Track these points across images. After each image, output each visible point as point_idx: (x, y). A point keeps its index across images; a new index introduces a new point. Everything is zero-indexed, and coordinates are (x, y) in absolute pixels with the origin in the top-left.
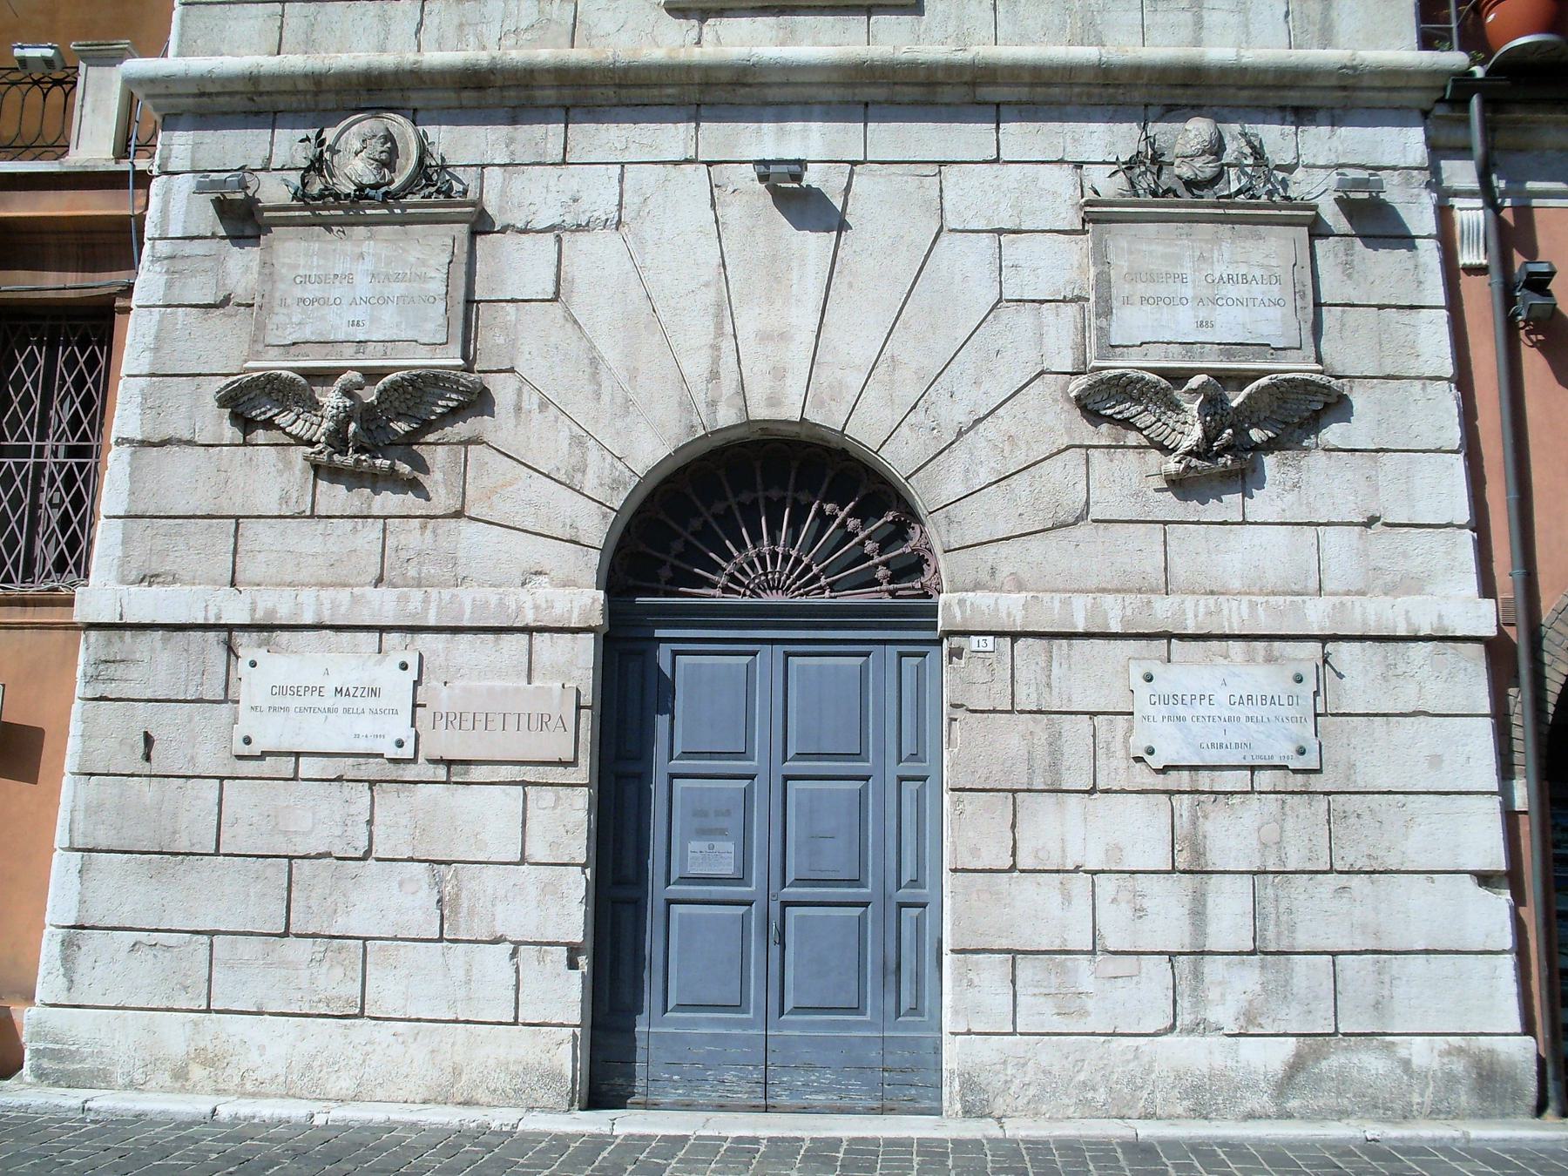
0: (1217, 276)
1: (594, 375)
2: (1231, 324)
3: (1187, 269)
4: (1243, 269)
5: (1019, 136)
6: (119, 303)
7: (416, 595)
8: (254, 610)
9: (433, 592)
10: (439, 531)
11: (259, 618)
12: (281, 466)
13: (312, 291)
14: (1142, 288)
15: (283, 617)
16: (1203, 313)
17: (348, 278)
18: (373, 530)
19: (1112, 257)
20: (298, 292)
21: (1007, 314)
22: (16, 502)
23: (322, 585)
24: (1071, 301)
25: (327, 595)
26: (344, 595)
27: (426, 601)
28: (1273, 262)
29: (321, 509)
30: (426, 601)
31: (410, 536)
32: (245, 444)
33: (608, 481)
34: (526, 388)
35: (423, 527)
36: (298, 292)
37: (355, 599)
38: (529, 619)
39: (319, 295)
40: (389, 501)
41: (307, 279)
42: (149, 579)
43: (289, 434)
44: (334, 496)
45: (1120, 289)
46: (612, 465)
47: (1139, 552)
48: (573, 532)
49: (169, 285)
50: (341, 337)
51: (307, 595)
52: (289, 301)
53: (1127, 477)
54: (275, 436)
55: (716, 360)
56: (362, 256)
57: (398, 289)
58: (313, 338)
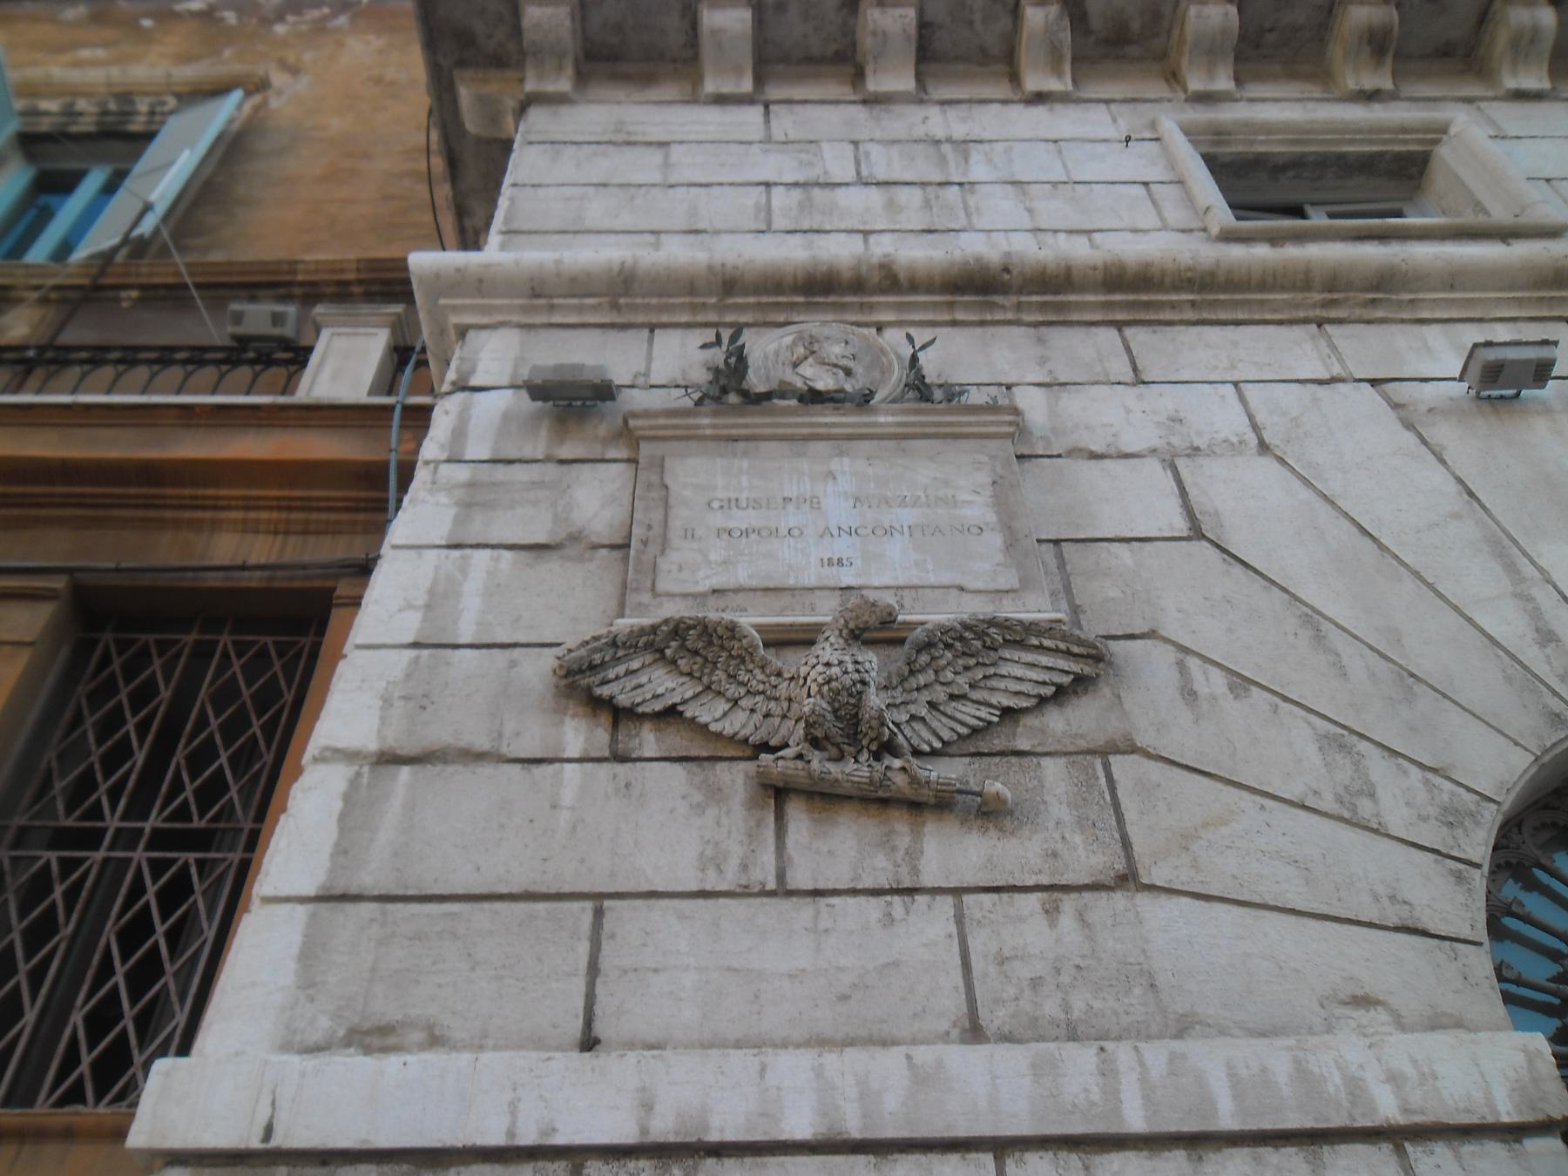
1: (1319, 638)
6: (343, 589)
7: (1080, 1060)
8: (647, 1107)
9: (1123, 1053)
10: (1092, 917)
11: (663, 1128)
12: (698, 797)
13: (741, 519)
15: (725, 1128)
17: (814, 503)
18: (931, 923)
20: (718, 520)
22: (40, 933)
23: (820, 1042)
25: (845, 1066)
26: (889, 1067)
27: (1107, 1071)
29: (800, 878)
30: (1107, 1071)
31: (1026, 930)
32: (620, 758)
33: (1433, 811)
34: (1193, 663)
35: (1051, 912)
36: (718, 520)
37: (921, 1078)
38: (1387, 1108)
39: (756, 524)
40: (951, 852)
41: (732, 503)
42: (373, 1037)
43: (719, 736)
44: (832, 849)
46: (1426, 782)
48: (1404, 912)
49: (458, 521)
50: (811, 580)
51: (793, 1068)
52: (699, 532)
54: (677, 741)
55: (1535, 613)
56: (831, 475)
57: (907, 516)
58: (754, 583)
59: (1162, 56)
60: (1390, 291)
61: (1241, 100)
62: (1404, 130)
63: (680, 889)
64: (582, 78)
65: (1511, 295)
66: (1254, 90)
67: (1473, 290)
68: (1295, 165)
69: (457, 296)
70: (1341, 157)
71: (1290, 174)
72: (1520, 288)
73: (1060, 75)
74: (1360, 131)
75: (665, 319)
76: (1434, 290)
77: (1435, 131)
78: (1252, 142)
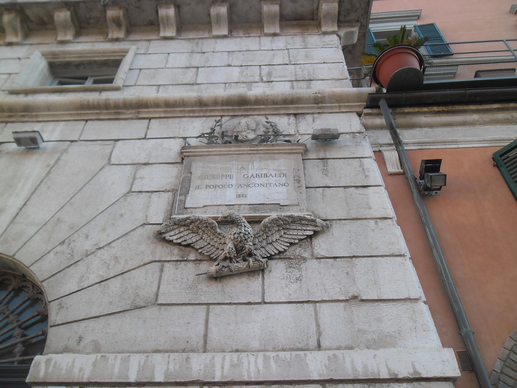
0: (250, 175)
2: (256, 195)
3: (234, 173)
4: (265, 172)
5: (157, 128)
14: (207, 182)
16: (240, 191)
19: (193, 170)
21: (133, 199)
24: (169, 191)
28: (282, 168)
45: (195, 182)
47: (187, 324)
53: (180, 279)
59: (81, 28)
60: (29, 112)
61: (75, 42)
62: (114, 52)
63: (282, 305)
64: (282, 27)
65: (67, 112)
66: (82, 39)
67: (56, 111)
68: (79, 65)
69: (300, 104)
70: (95, 62)
71: (82, 67)
72: (72, 110)
73: (16, 35)
74: (101, 53)
75: (300, 112)
76: (43, 111)
77: (122, 52)
78: (65, 58)
